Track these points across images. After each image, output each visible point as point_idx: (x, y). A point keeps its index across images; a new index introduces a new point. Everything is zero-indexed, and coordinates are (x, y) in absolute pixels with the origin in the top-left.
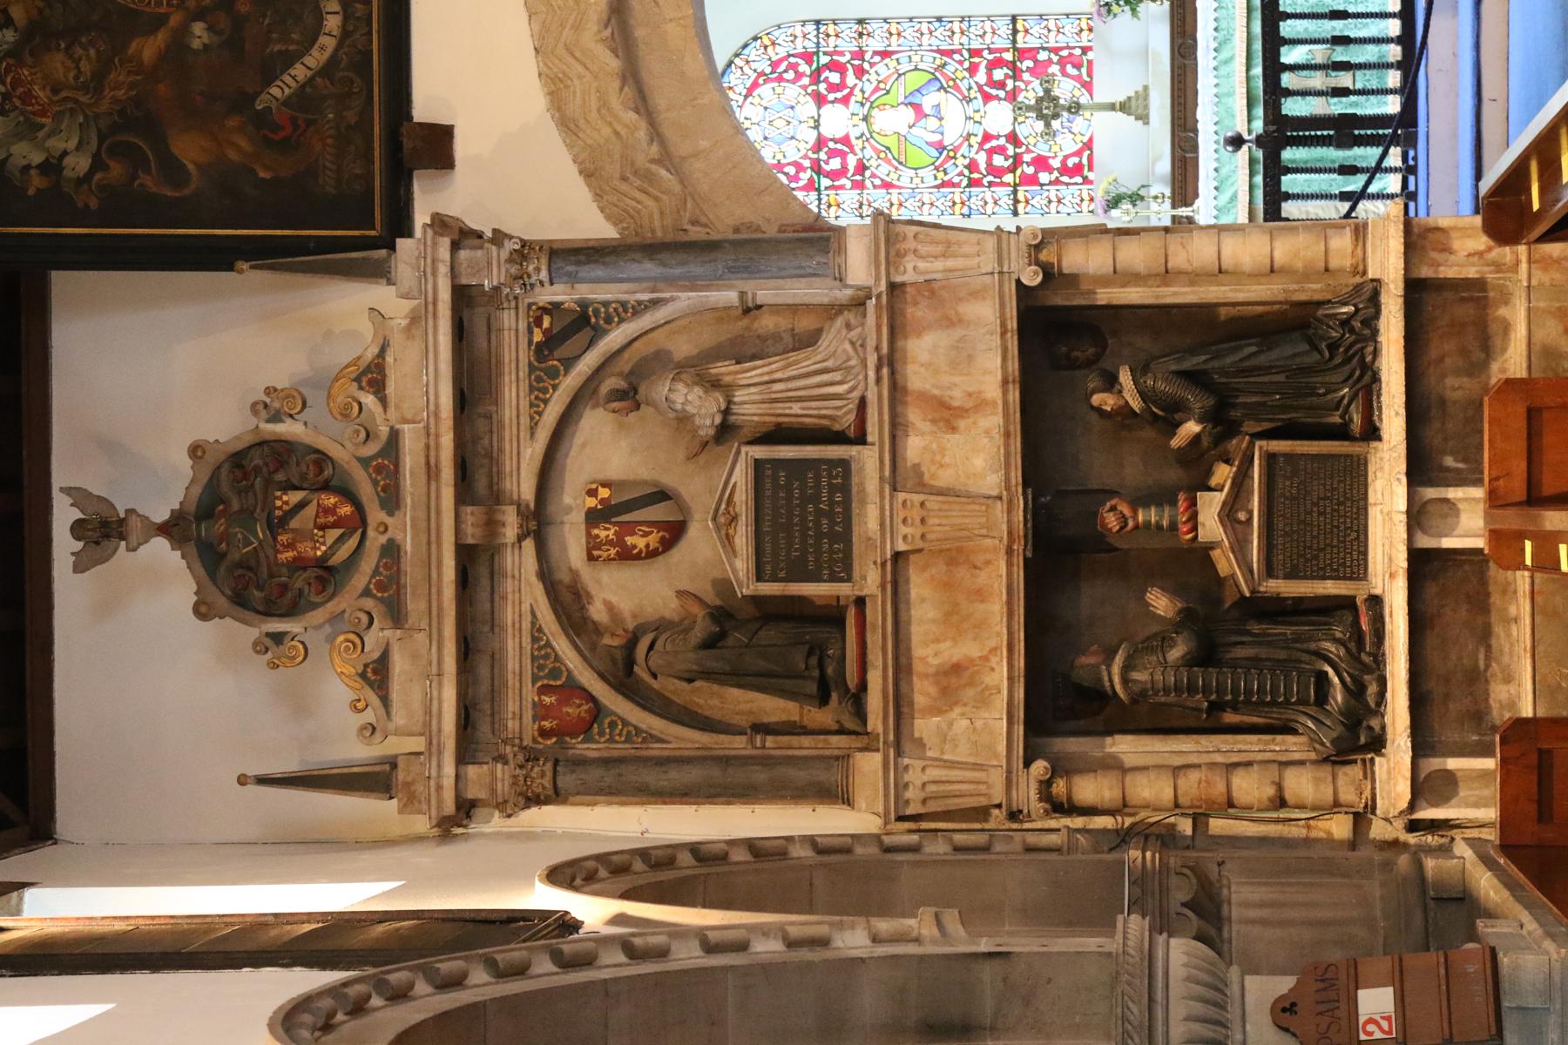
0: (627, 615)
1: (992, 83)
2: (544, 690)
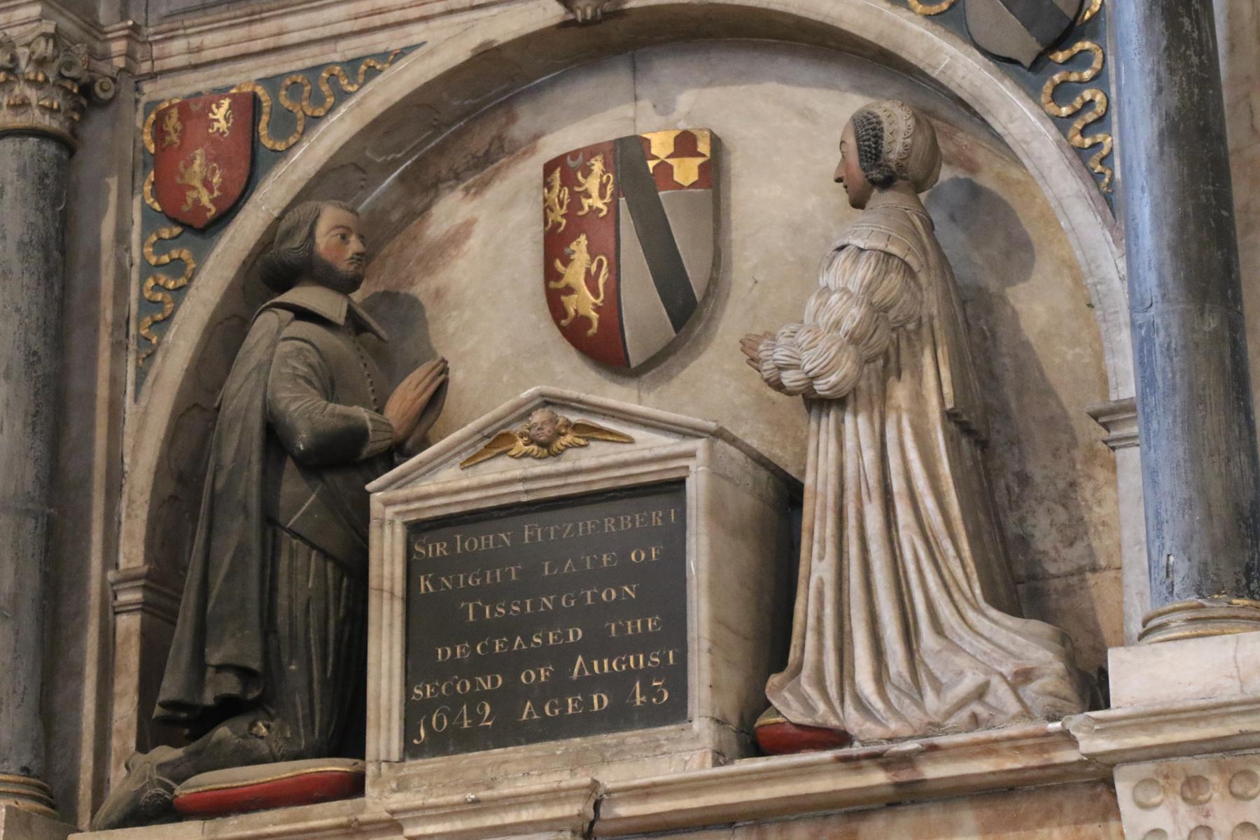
0: (440, 278)
2: (248, 108)
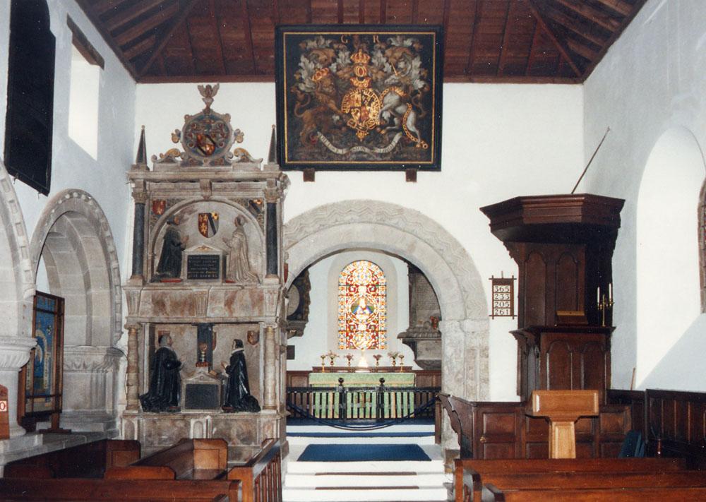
1: (371, 326)
2: (164, 202)
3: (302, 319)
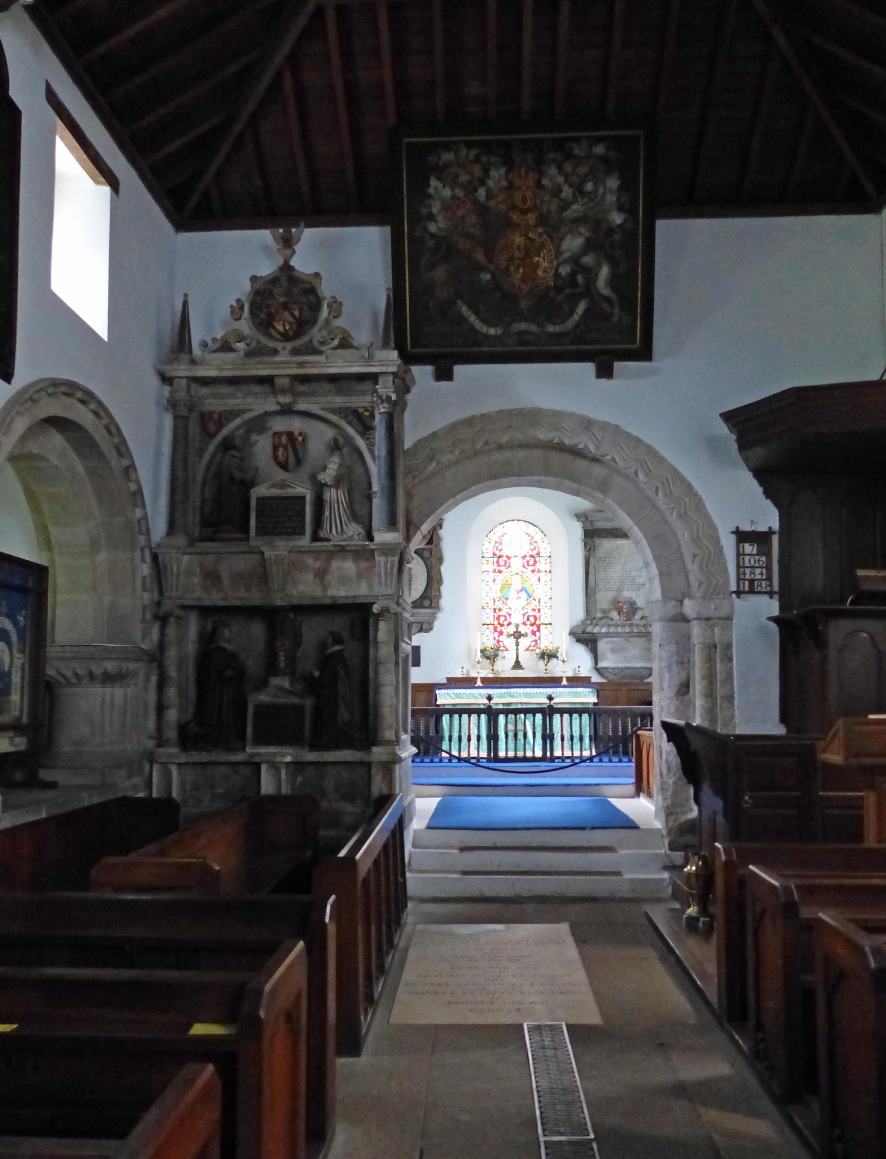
3: (430, 607)
